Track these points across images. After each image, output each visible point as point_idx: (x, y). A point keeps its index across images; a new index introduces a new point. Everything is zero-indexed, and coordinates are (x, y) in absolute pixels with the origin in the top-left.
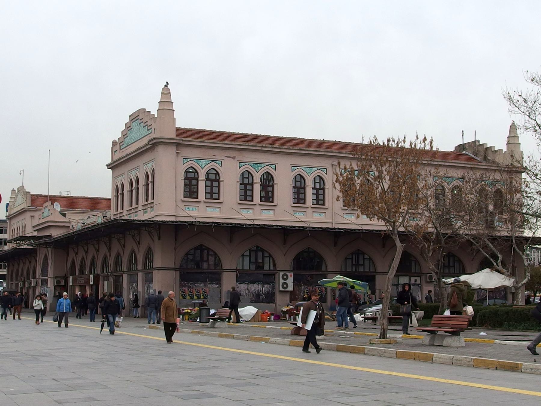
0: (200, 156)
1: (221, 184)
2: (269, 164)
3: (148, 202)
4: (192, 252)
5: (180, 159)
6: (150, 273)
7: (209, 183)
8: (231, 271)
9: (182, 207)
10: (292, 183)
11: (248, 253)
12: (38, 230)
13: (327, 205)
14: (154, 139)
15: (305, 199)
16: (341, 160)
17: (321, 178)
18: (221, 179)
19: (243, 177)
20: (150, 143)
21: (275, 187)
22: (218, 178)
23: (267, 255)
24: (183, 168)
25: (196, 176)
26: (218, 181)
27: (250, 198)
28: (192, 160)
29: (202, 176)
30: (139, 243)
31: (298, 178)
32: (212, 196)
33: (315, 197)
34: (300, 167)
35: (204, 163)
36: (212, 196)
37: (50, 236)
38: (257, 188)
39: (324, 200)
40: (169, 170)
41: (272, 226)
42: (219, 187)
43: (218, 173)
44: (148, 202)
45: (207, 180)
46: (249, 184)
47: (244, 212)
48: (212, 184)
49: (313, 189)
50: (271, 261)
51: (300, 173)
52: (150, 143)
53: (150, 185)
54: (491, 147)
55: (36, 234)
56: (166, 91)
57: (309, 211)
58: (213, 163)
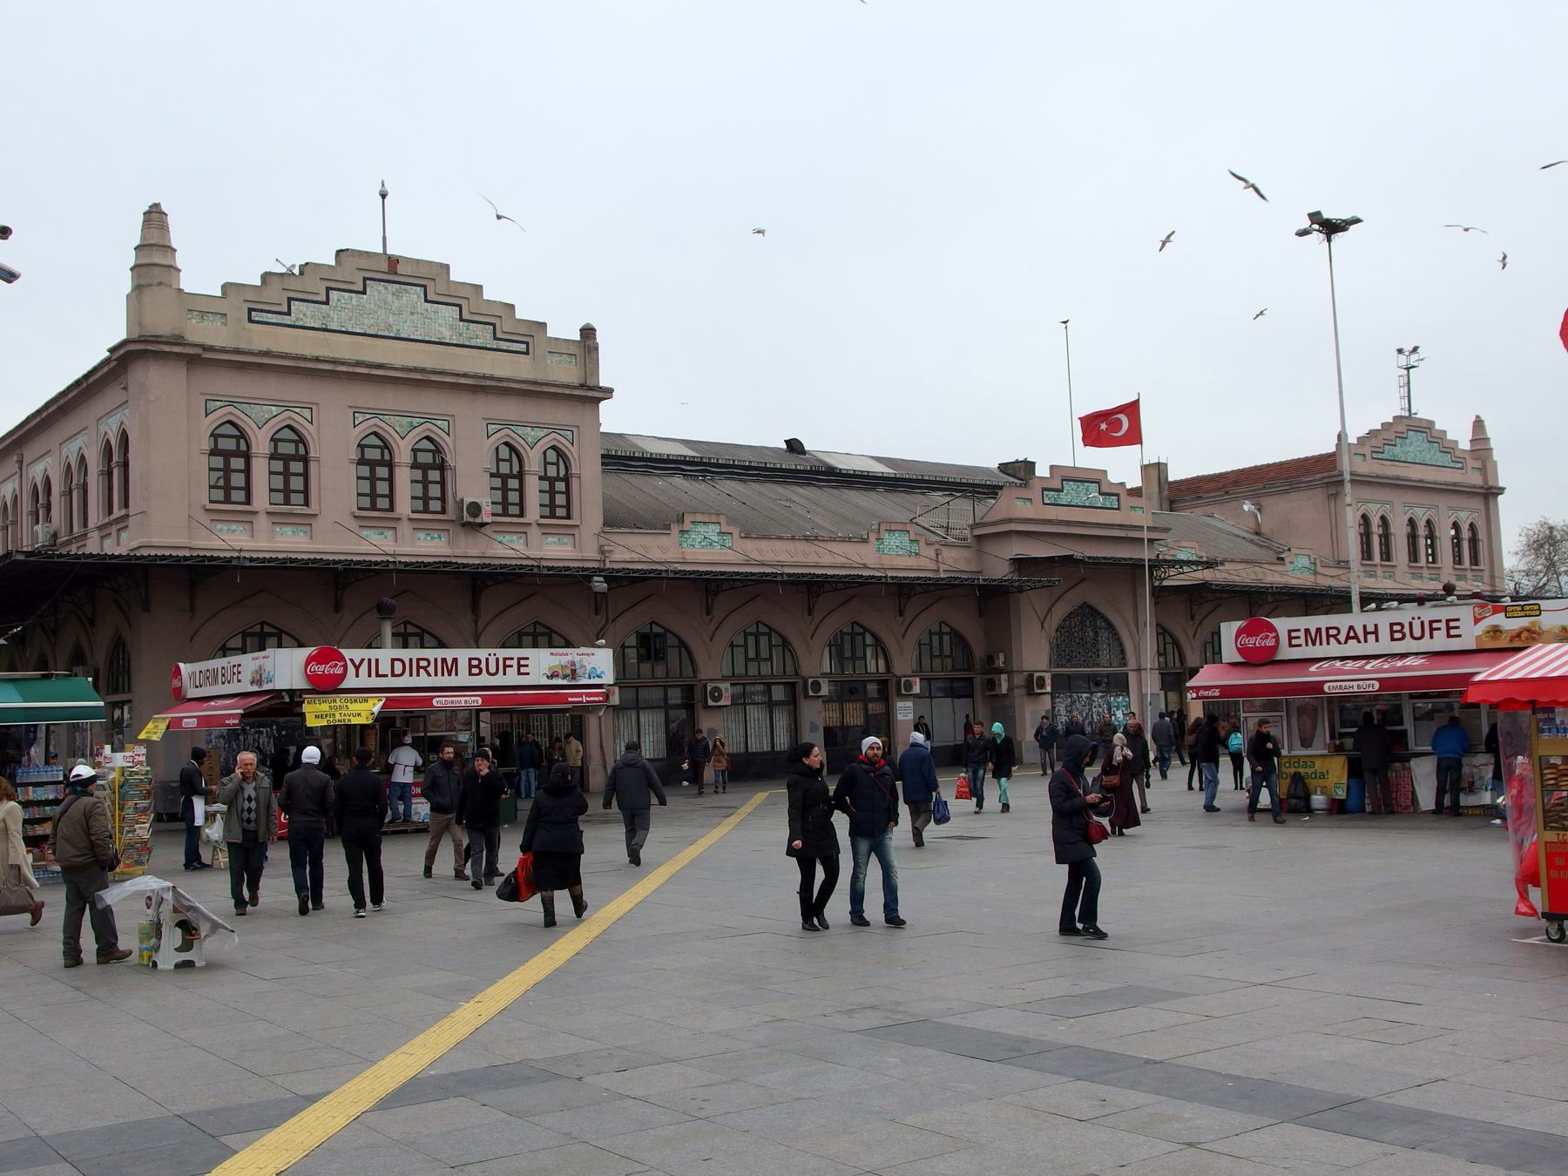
1: (313, 466)
3: (113, 517)
6: (124, 703)
7: (278, 466)
9: (208, 524)
11: (740, 640)
17: (560, 454)
18: (312, 454)
21: (574, 483)
22: (387, 457)
24: (208, 424)
25: (302, 451)
26: (305, 460)
29: (261, 444)
30: (92, 622)
31: (552, 456)
32: (426, 505)
33: (546, 499)
34: (554, 430)
35: (532, 434)
36: (426, 505)
38: (404, 478)
39: (568, 507)
40: (170, 433)
41: (738, 574)
42: (306, 475)
43: (301, 440)
44: (113, 517)
45: (415, 465)
46: (512, 476)
47: (373, 536)
48: (373, 472)
49: (492, 475)
50: (1169, 639)
53: (115, 472)
57: (405, 528)
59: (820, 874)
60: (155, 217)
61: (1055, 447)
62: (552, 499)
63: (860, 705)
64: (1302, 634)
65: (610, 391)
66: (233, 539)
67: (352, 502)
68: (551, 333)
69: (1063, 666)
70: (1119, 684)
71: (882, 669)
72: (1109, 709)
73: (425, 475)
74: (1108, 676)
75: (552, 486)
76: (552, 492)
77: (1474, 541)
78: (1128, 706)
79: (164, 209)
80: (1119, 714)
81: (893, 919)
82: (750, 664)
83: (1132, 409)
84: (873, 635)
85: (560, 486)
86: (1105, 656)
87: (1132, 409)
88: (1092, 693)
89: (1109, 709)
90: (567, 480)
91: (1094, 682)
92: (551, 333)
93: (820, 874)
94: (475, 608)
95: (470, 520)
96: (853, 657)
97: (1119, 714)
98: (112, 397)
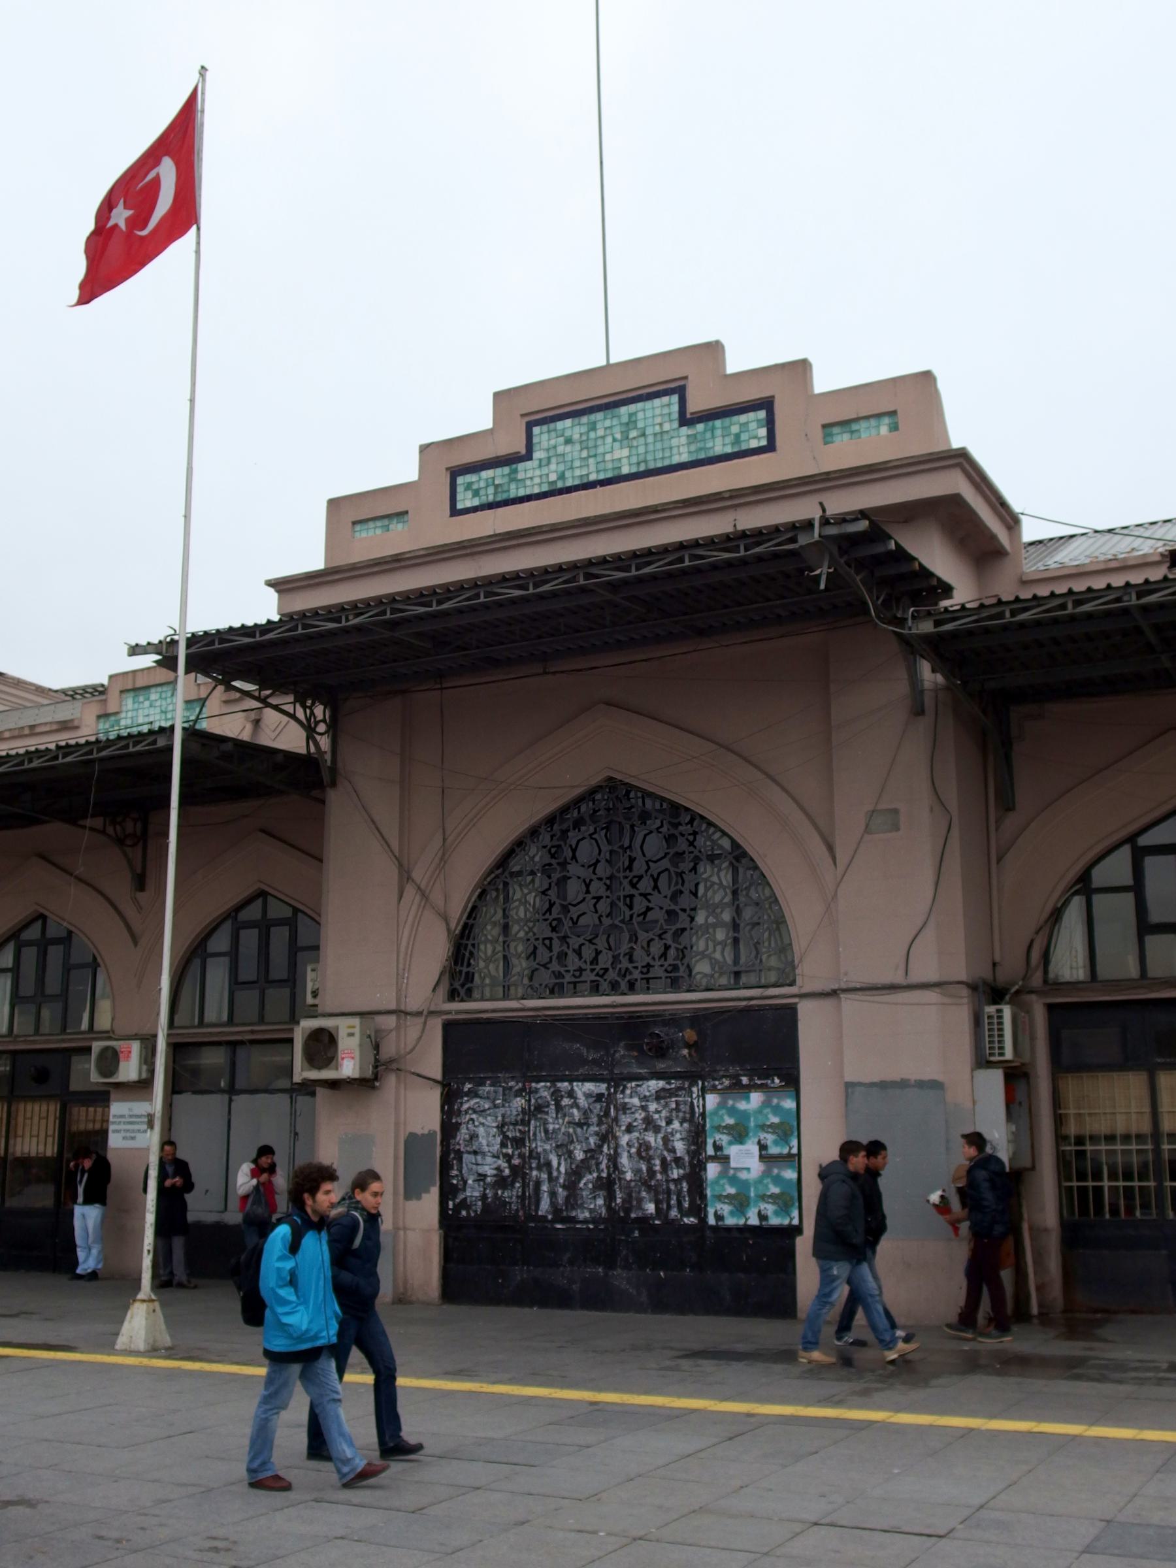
63: (54, 1108)
64: (680, 887)
68: (822, 383)
69: (556, 990)
70: (761, 1048)
72: (697, 1136)
74: (698, 1019)
78: (790, 1128)
79: (133, 644)
80: (745, 1158)
81: (393, 1444)
82: (242, 996)
83: (203, 67)
86: (709, 951)
87: (203, 67)
88: (618, 1081)
89: (697, 1136)
91: (637, 1042)
92: (822, 383)
97: (745, 1158)
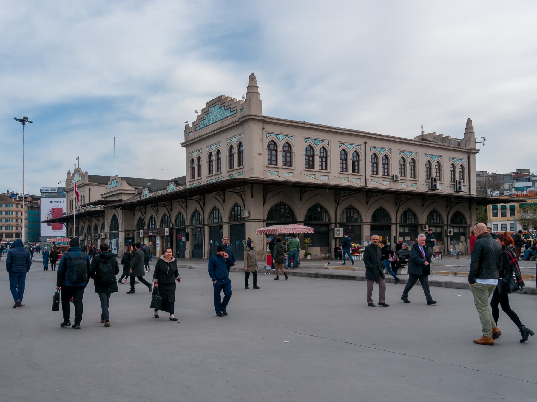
0: (278, 132)
2: (324, 141)
4: (345, 211)
5: (265, 133)
8: (367, 223)
10: (339, 156)
12: (105, 197)
13: (329, 171)
14: (246, 116)
15: (276, 160)
16: (368, 141)
19: (307, 150)
20: (240, 120)
21: (329, 158)
23: (324, 210)
24: (267, 141)
27: (274, 162)
28: (273, 134)
31: (309, 148)
35: (281, 137)
37: (121, 200)
38: (280, 155)
46: (324, 157)
51: (287, 141)
52: (240, 120)
54: (448, 137)
55: (103, 199)
56: (469, 122)
58: (287, 138)
59: (222, 295)
60: (469, 122)
61: (196, 115)
62: (271, 157)
65: (479, 150)
66: (273, 175)
67: (339, 170)
71: (327, 221)
73: (271, 152)
75: (322, 159)
76: (322, 161)
77: (240, 153)
84: (288, 207)
85: (274, 153)
90: (326, 157)
93: (222, 295)
94: (470, 208)
95: (394, 179)
96: (409, 219)
98: (239, 131)
